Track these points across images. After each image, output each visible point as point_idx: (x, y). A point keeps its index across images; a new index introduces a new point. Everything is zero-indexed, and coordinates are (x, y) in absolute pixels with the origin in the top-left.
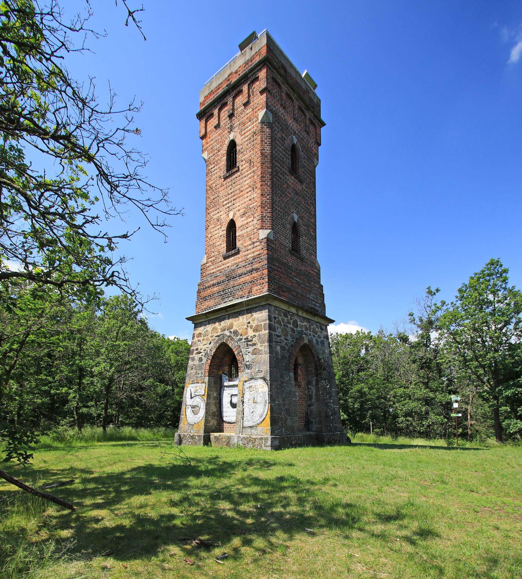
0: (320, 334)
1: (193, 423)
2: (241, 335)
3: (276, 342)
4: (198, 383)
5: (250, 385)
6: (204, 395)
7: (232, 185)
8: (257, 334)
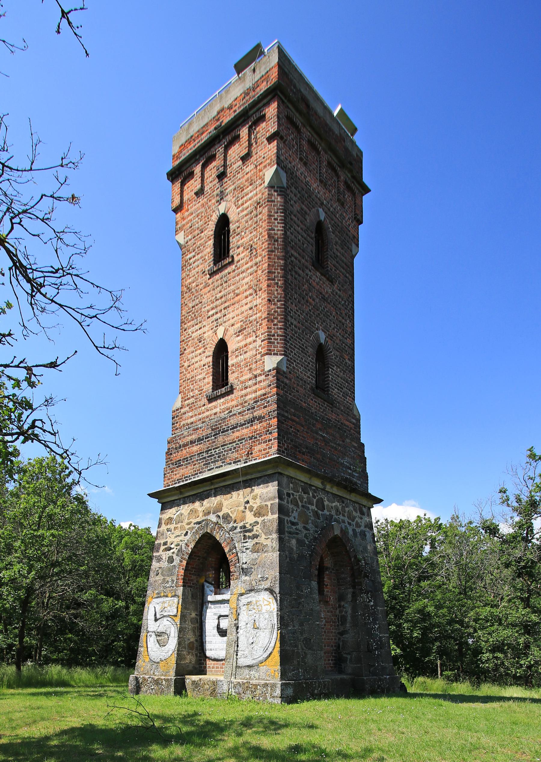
2: (235, 521)
3: (290, 533)
4: (167, 596)
5: (249, 600)
6: (176, 616)
8: (260, 520)
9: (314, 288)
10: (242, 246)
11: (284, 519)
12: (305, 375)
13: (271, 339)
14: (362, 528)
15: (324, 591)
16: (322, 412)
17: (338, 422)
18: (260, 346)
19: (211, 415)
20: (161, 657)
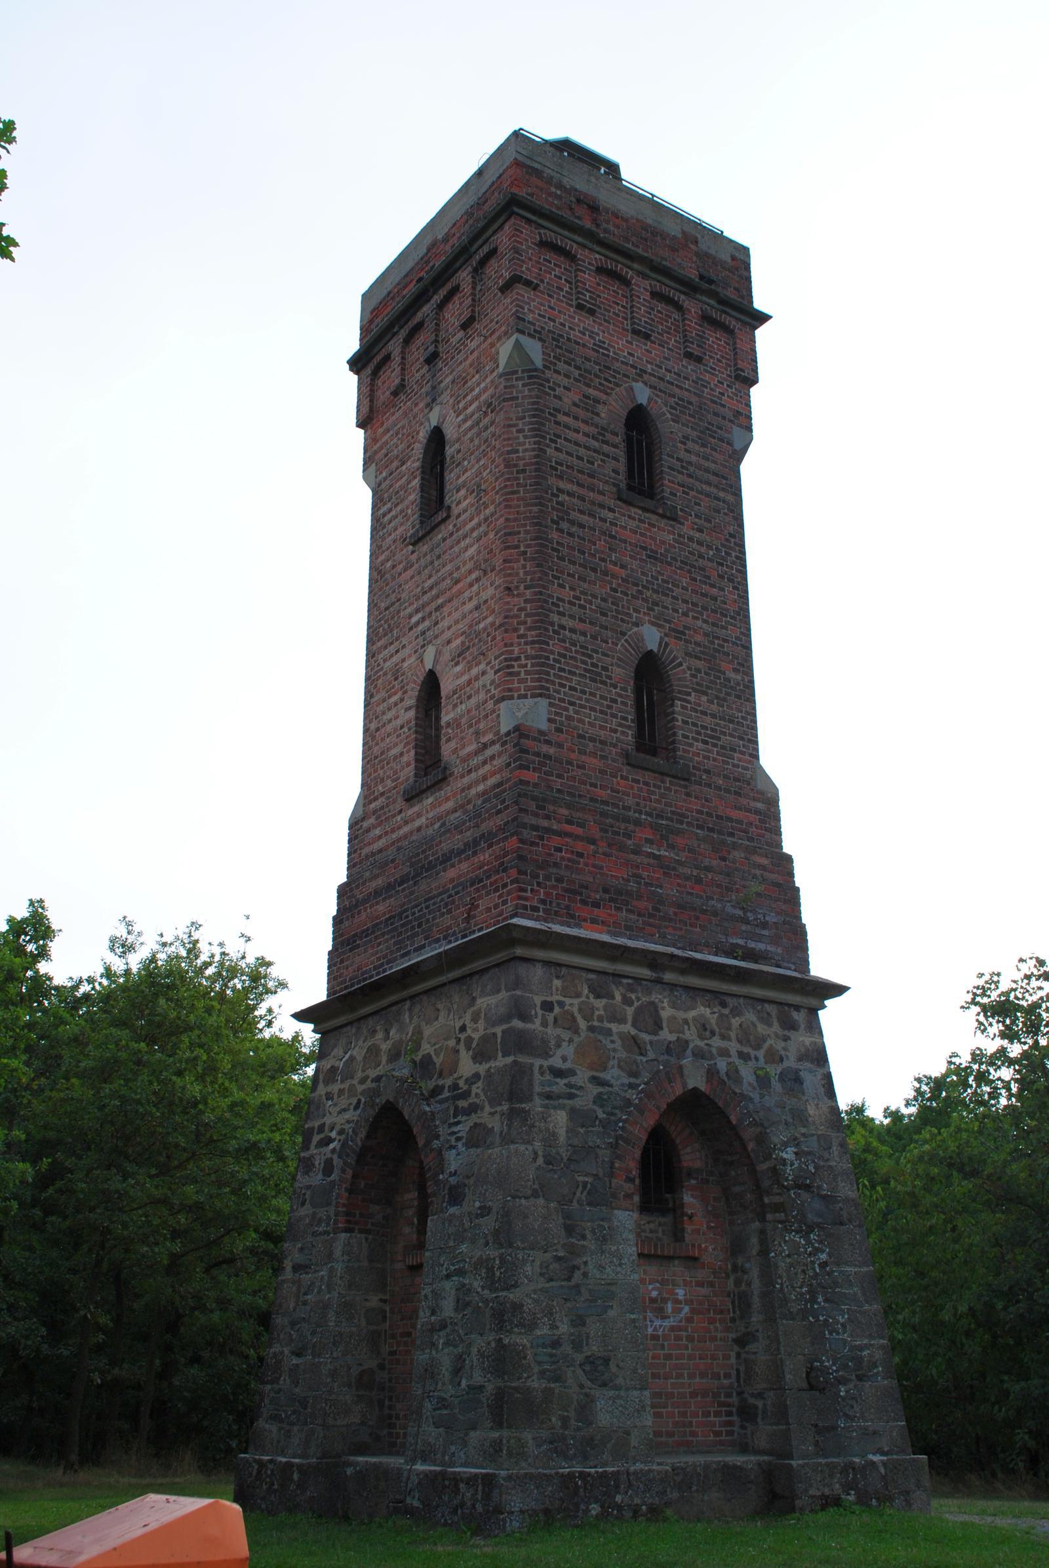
0: (780, 1045)
3: (549, 1096)
7: (432, 563)
9: (625, 542)
10: (464, 486)
11: (532, 1065)
12: (604, 728)
13: (513, 667)
14: (791, 1062)
15: (683, 1230)
16: (658, 801)
17: (709, 814)
18: (492, 682)
19: (411, 833)
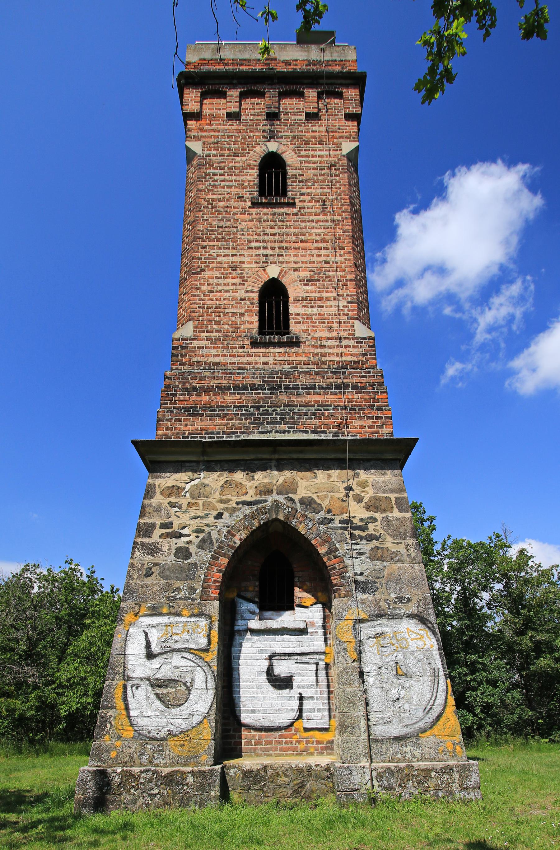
1: (162, 734)
2: (329, 511)
4: (178, 614)
5: (379, 630)
6: (206, 650)
8: (379, 516)
20: (171, 728)
